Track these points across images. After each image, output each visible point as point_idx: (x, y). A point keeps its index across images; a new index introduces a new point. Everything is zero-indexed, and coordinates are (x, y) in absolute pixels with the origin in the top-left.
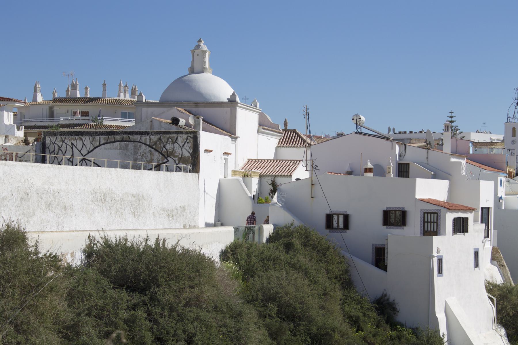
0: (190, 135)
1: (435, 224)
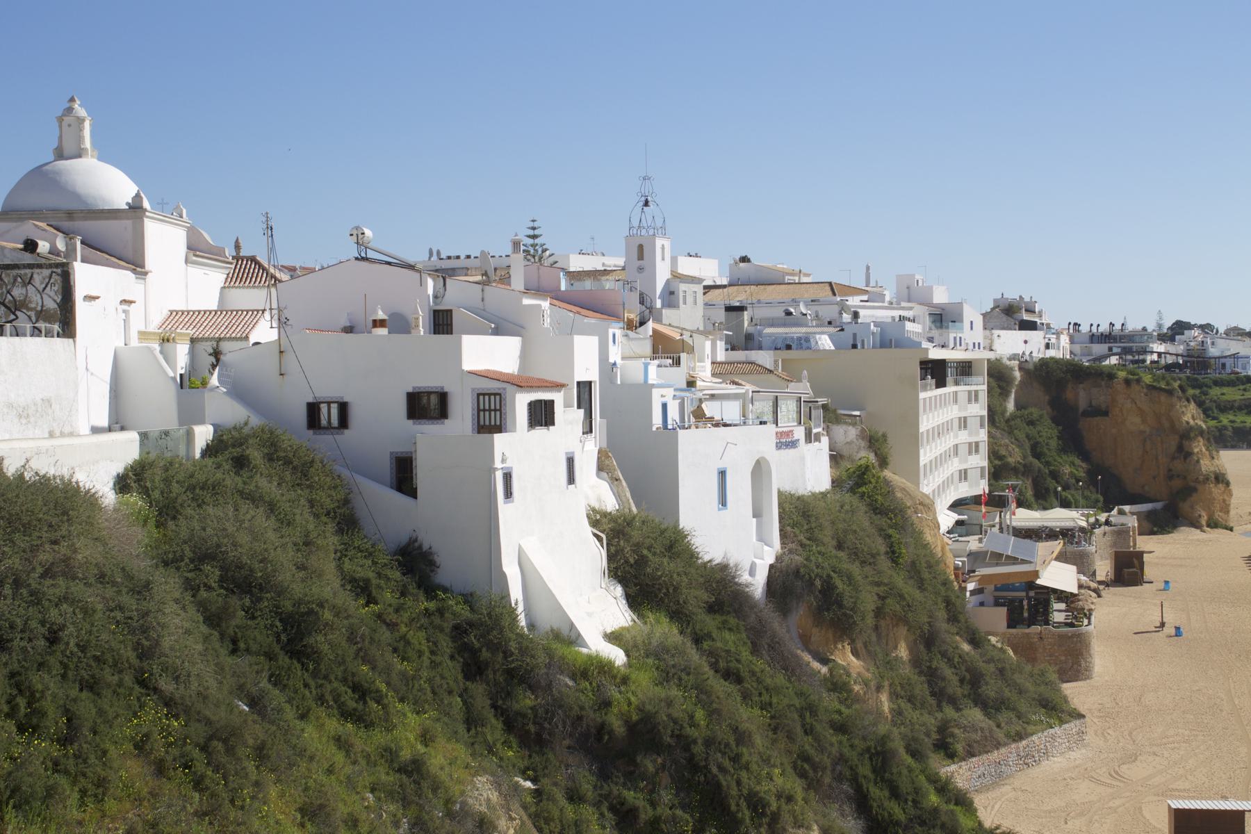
0: (55, 270)
1: (498, 413)
